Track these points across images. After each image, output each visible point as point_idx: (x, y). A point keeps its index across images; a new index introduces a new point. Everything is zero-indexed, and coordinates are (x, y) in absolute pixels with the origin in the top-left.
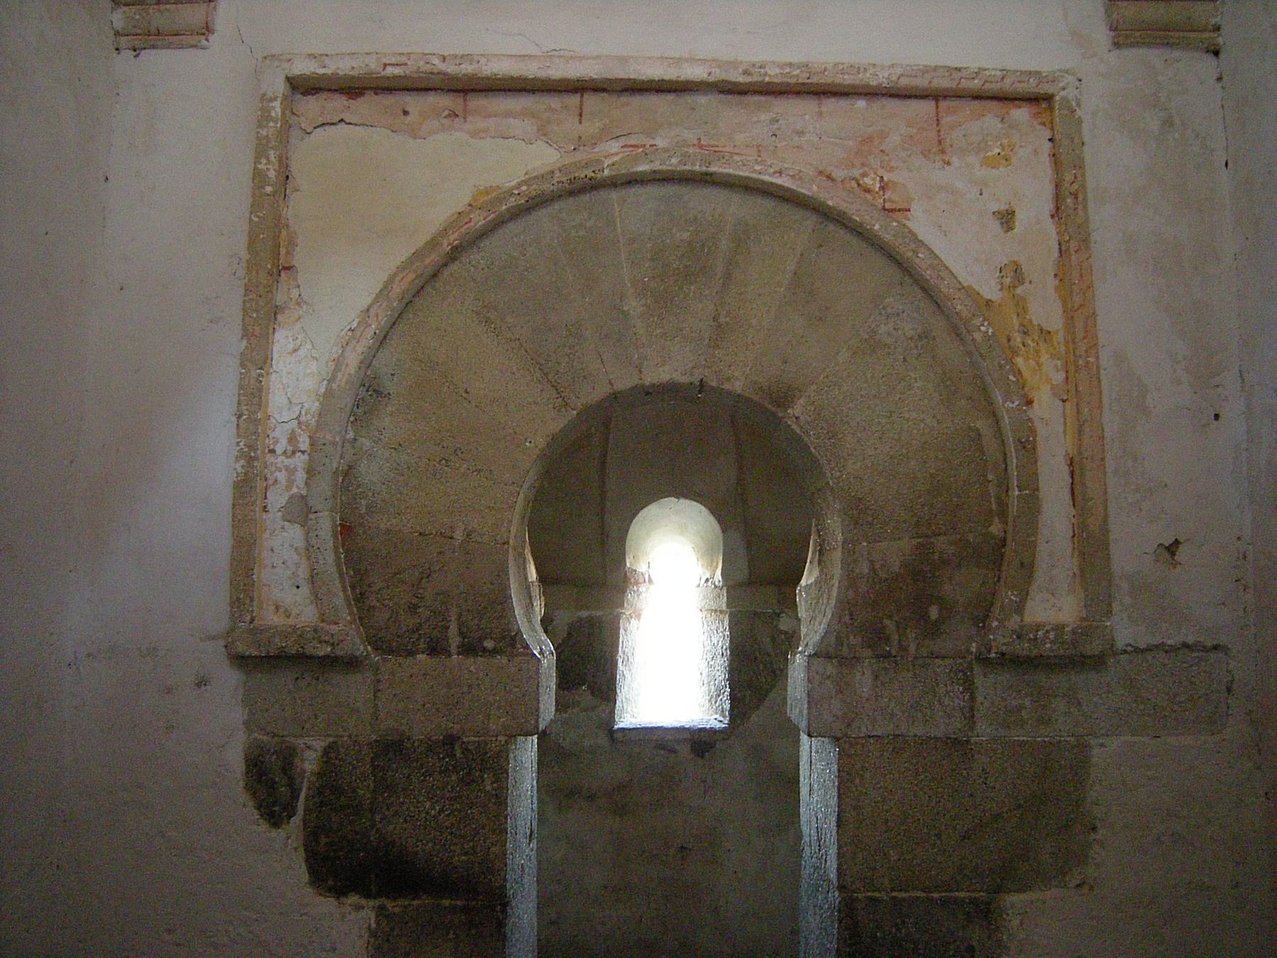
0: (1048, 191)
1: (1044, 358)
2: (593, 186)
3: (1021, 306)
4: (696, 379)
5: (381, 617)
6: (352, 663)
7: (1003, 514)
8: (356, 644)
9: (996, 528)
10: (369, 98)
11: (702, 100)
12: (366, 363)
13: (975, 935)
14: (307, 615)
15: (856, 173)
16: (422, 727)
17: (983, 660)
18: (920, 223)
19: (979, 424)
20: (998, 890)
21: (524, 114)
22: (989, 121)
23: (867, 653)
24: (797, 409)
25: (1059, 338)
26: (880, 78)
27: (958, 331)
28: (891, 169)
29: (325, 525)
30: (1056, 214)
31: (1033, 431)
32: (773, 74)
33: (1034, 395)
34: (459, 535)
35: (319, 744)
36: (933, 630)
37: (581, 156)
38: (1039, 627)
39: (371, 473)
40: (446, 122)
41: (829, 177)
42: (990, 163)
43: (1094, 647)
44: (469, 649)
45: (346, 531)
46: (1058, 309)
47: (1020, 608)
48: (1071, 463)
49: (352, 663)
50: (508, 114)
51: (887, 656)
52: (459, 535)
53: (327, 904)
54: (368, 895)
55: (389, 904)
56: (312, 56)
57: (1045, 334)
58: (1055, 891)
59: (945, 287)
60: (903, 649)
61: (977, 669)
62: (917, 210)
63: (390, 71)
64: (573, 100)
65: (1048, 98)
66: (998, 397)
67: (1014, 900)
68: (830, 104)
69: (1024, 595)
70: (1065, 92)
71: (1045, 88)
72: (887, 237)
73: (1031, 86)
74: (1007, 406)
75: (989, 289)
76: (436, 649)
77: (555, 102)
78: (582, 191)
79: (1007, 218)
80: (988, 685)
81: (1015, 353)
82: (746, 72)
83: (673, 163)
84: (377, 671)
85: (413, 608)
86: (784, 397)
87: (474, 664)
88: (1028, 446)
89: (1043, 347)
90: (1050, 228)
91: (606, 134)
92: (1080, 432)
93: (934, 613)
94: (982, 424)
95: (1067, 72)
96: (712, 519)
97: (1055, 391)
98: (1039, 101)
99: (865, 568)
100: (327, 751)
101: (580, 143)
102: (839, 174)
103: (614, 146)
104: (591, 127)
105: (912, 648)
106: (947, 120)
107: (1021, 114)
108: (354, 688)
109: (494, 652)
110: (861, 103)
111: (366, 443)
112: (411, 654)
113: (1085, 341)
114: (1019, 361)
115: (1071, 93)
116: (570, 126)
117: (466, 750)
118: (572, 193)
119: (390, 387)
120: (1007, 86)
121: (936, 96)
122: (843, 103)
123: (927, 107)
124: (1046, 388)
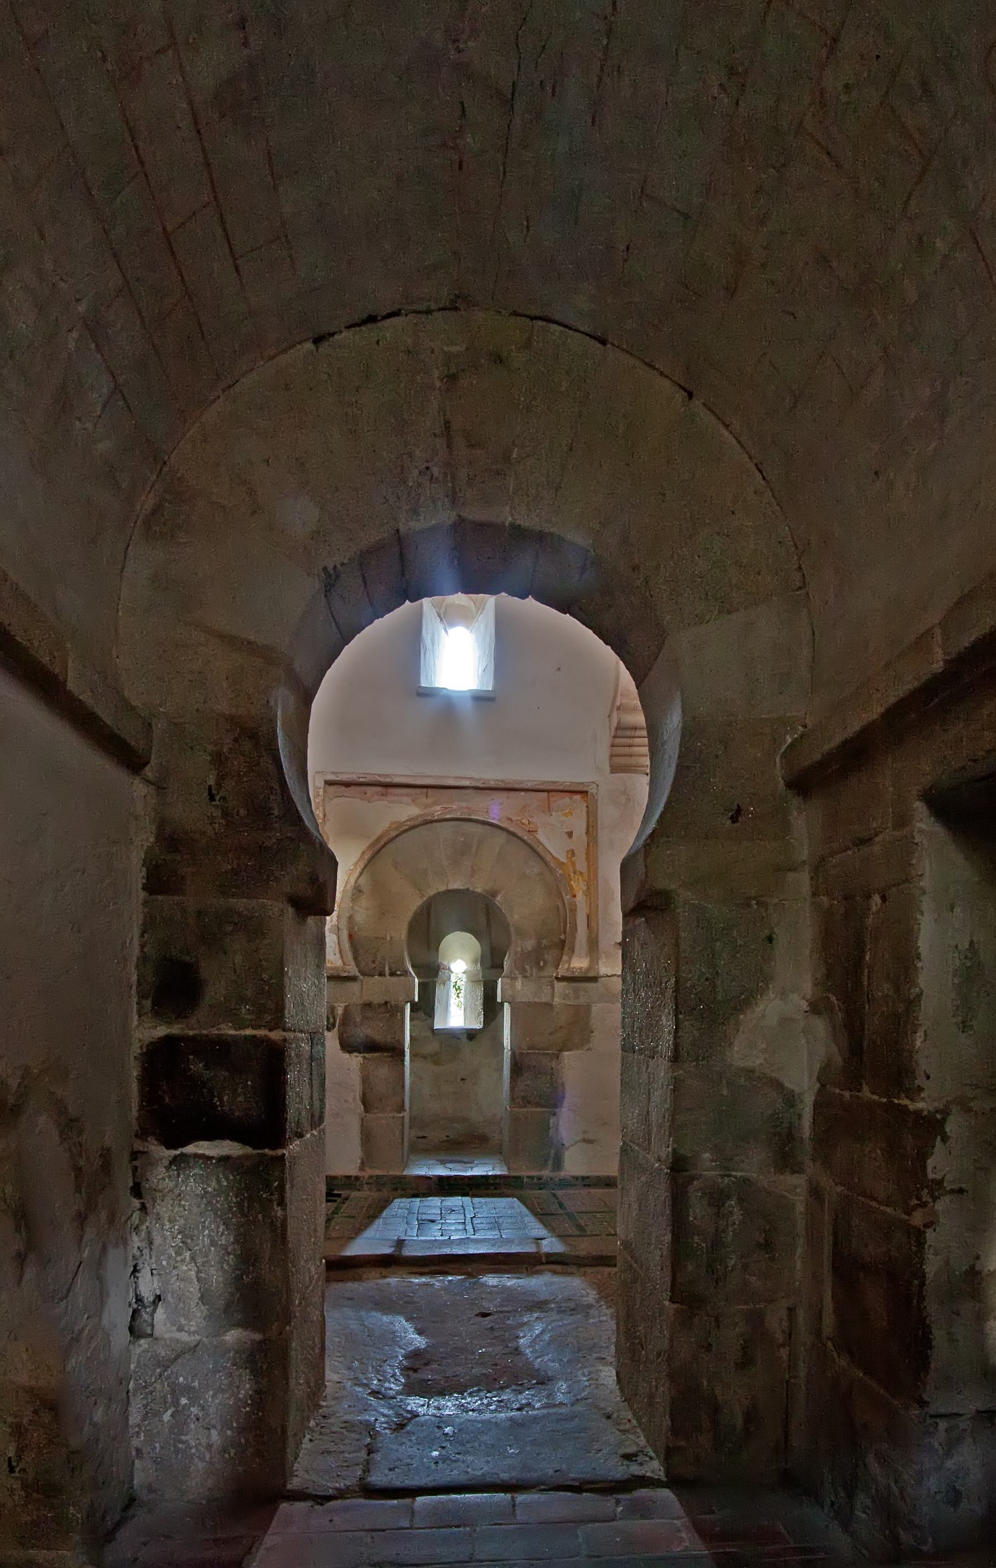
0: (584, 824)
1: (581, 881)
2: (432, 822)
3: (573, 864)
4: (466, 887)
5: (363, 964)
6: (353, 979)
7: (565, 933)
8: (353, 970)
9: (562, 937)
10: (352, 787)
11: (469, 791)
12: (356, 882)
13: (554, 1064)
14: (339, 963)
15: (519, 818)
16: (377, 999)
17: (557, 978)
18: (541, 836)
19: (558, 903)
20: (562, 1050)
21: (407, 795)
22: (566, 800)
23: (520, 976)
24: (499, 898)
25: (586, 875)
26: (529, 785)
27: (551, 871)
28: (532, 817)
29: (345, 935)
30: (587, 833)
31: (576, 906)
32: (492, 784)
33: (577, 893)
34: (388, 938)
35: (343, 1005)
36: (541, 969)
37: (427, 811)
38: (574, 968)
39: (360, 918)
40: (381, 797)
41: (511, 820)
42: (565, 815)
43: (591, 974)
44: (392, 974)
45: (351, 937)
46: (585, 865)
47: (569, 962)
48: (588, 916)
49: (353, 979)
50: (404, 795)
51: (526, 977)
52: (388, 938)
53: (347, 1056)
54: (360, 1053)
55: (367, 1055)
56: (333, 773)
57: (581, 873)
58: (580, 1052)
59: (548, 858)
60: (531, 975)
61: (555, 982)
62: (540, 831)
63: (361, 780)
64: (425, 790)
65: (587, 792)
66: (564, 894)
67: (566, 1053)
68: (512, 794)
69: (570, 959)
70: (592, 790)
71: (585, 789)
72: (529, 841)
73: (580, 788)
74: (567, 898)
75: (563, 859)
76: (382, 974)
77: (418, 791)
78: (427, 823)
79: (570, 834)
80: (559, 986)
81: (571, 880)
82: (483, 783)
83: (458, 815)
84: (362, 981)
85: (374, 962)
86: (494, 894)
87: (394, 979)
88: (574, 911)
89: (580, 878)
90: (585, 838)
91: (435, 803)
92: (590, 906)
93: (542, 964)
94: (559, 904)
95: (593, 782)
96: (480, 953)
97: (584, 892)
98: (584, 793)
99: (519, 949)
100: (346, 1007)
101: (426, 806)
102: (514, 818)
103: (438, 808)
104: (430, 801)
105: (534, 975)
106: (552, 799)
107: (577, 797)
108: (354, 987)
109: (401, 975)
110: (523, 793)
111: (357, 908)
112: (373, 976)
113: (834, 264)
114: (572, 883)
115: (594, 791)
116: (423, 800)
117: (391, 1006)
118: (424, 824)
119: (364, 889)
120: (572, 788)
121: (548, 791)
122: (517, 793)
123: (545, 794)
124: (581, 892)
